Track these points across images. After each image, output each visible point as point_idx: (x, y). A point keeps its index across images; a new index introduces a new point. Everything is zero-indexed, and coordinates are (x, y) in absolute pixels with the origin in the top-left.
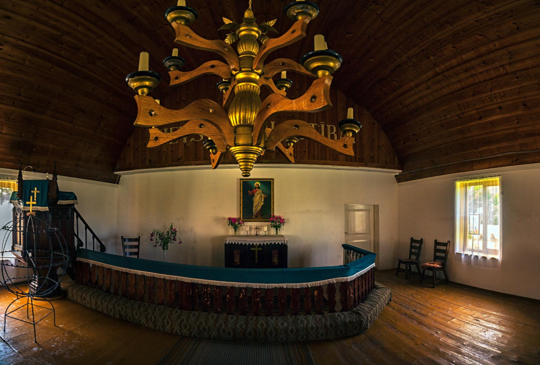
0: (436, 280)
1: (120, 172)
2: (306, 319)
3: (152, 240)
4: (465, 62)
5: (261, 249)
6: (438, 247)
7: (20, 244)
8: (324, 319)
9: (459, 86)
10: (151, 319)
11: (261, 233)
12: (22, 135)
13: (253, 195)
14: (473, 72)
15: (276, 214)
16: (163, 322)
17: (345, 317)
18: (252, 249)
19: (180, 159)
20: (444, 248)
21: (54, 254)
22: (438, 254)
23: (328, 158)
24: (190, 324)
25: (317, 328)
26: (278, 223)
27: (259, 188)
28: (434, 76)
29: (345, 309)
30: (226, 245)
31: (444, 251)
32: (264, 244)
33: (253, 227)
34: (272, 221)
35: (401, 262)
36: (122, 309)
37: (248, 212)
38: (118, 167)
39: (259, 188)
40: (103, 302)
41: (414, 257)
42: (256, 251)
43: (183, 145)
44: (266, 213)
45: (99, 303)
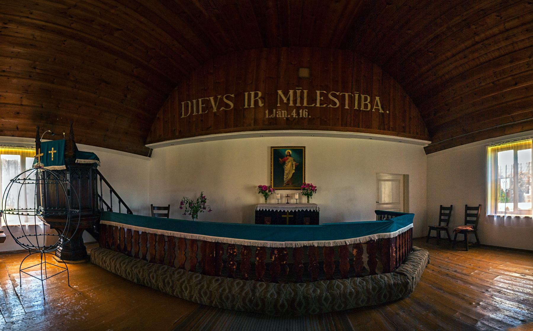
0: (469, 243)
1: (151, 145)
2: (343, 283)
3: (181, 208)
4: (507, 30)
5: (292, 216)
6: (468, 212)
8: (365, 283)
9: (497, 54)
10: (169, 283)
13: (284, 163)
14: (514, 39)
15: (307, 182)
16: (181, 287)
17: (389, 278)
18: (283, 216)
20: (475, 212)
21: (76, 220)
22: (468, 219)
24: (211, 292)
25: (357, 292)
26: (310, 191)
27: (290, 156)
28: (473, 45)
29: (386, 270)
30: (256, 211)
31: (476, 215)
33: (284, 195)
34: (304, 189)
35: (432, 228)
36: (140, 272)
39: (290, 156)
40: (133, 268)
41: (443, 224)
42: (288, 218)
44: (298, 181)
45: (118, 266)
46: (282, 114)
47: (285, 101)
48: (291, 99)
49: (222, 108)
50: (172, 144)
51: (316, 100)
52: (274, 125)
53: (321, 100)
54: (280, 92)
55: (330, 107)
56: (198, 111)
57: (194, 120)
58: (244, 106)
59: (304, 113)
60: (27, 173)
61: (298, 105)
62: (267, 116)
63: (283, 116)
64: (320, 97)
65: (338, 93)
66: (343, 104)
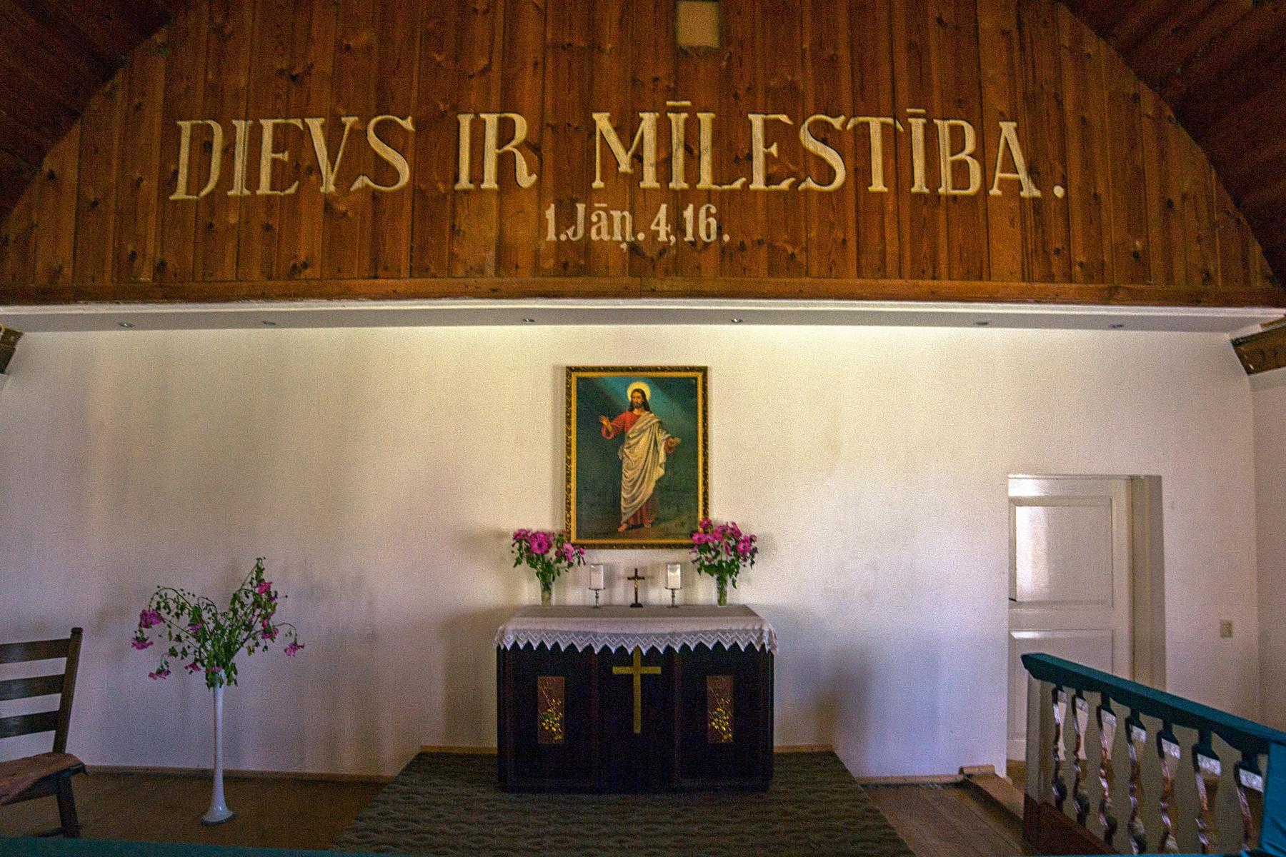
11: (657, 595)
13: (621, 437)
15: (720, 513)
19: (305, 266)
23: (943, 268)
26: (729, 551)
30: (501, 653)
32: (669, 649)
33: (622, 572)
34: (703, 547)
37: (600, 509)
39: (645, 406)
42: (637, 681)
43: (319, 210)
44: (678, 513)
46: (610, 227)
47: (625, 167)
48: (649, 155)
49: (362, 182)
51: (750, 157)
52: (574, 274)
53: (768, 156)
54: (602, 121)
55: (807, 191)
58: (457, 179)
59: (701, 223)
61: (678, 183)
62: (551, 235)
63: (618, 237)
64: (767, 146)
65: (837, 123)
66: (860, 173)
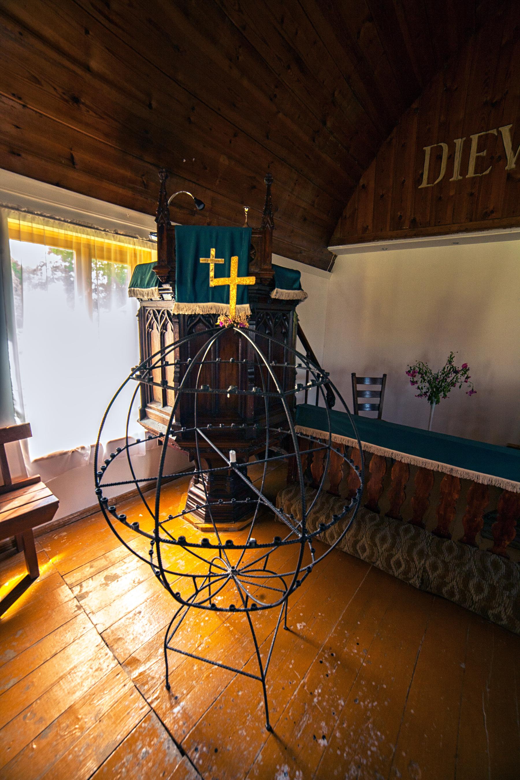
7: (165, 404)
12: (154, 104)
19: (492, 212)
38: (338, 235)
40: (377, 540)
50: (384, 248)
56: (464, 170)
57: (452, 193)
60: (207, 583)
